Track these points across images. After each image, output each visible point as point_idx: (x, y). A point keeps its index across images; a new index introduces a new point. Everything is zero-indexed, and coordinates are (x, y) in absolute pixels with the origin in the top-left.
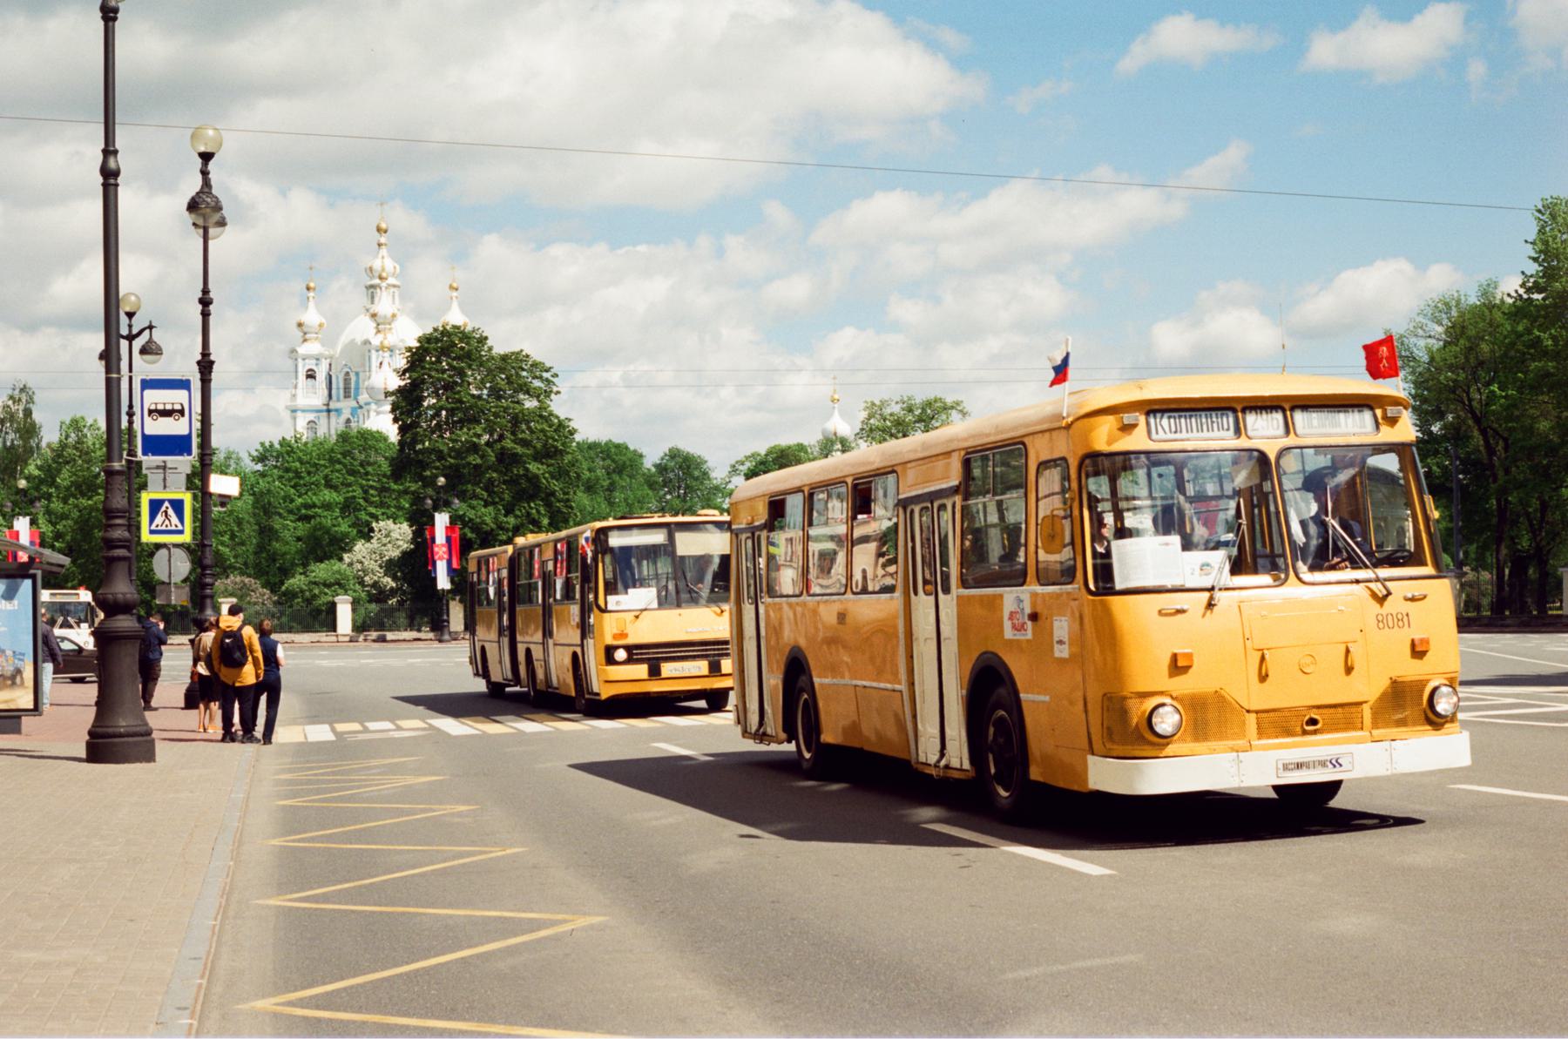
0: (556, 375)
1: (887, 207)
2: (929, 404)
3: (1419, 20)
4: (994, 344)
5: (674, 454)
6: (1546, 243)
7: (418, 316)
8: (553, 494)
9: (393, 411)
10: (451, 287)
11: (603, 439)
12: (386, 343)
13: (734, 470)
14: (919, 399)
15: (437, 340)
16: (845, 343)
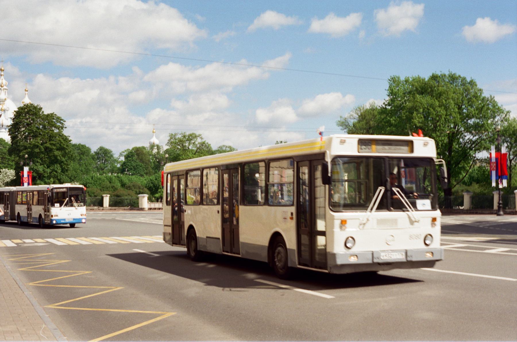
0: (65, 121)
1: (172, 69)
2: (191, 135)
3: (348, 18)
4: (207, 115)
5: (101, 149)
6: (392, 90)
7: (14, 100)
8: (63, 162)
9: (9, 131)
10: (25, 90)
11: (78, 143)
12: (3, 108)
13: (121, 155)
14: (187, 134)
15: (25, 108)
16: (157, 113)
